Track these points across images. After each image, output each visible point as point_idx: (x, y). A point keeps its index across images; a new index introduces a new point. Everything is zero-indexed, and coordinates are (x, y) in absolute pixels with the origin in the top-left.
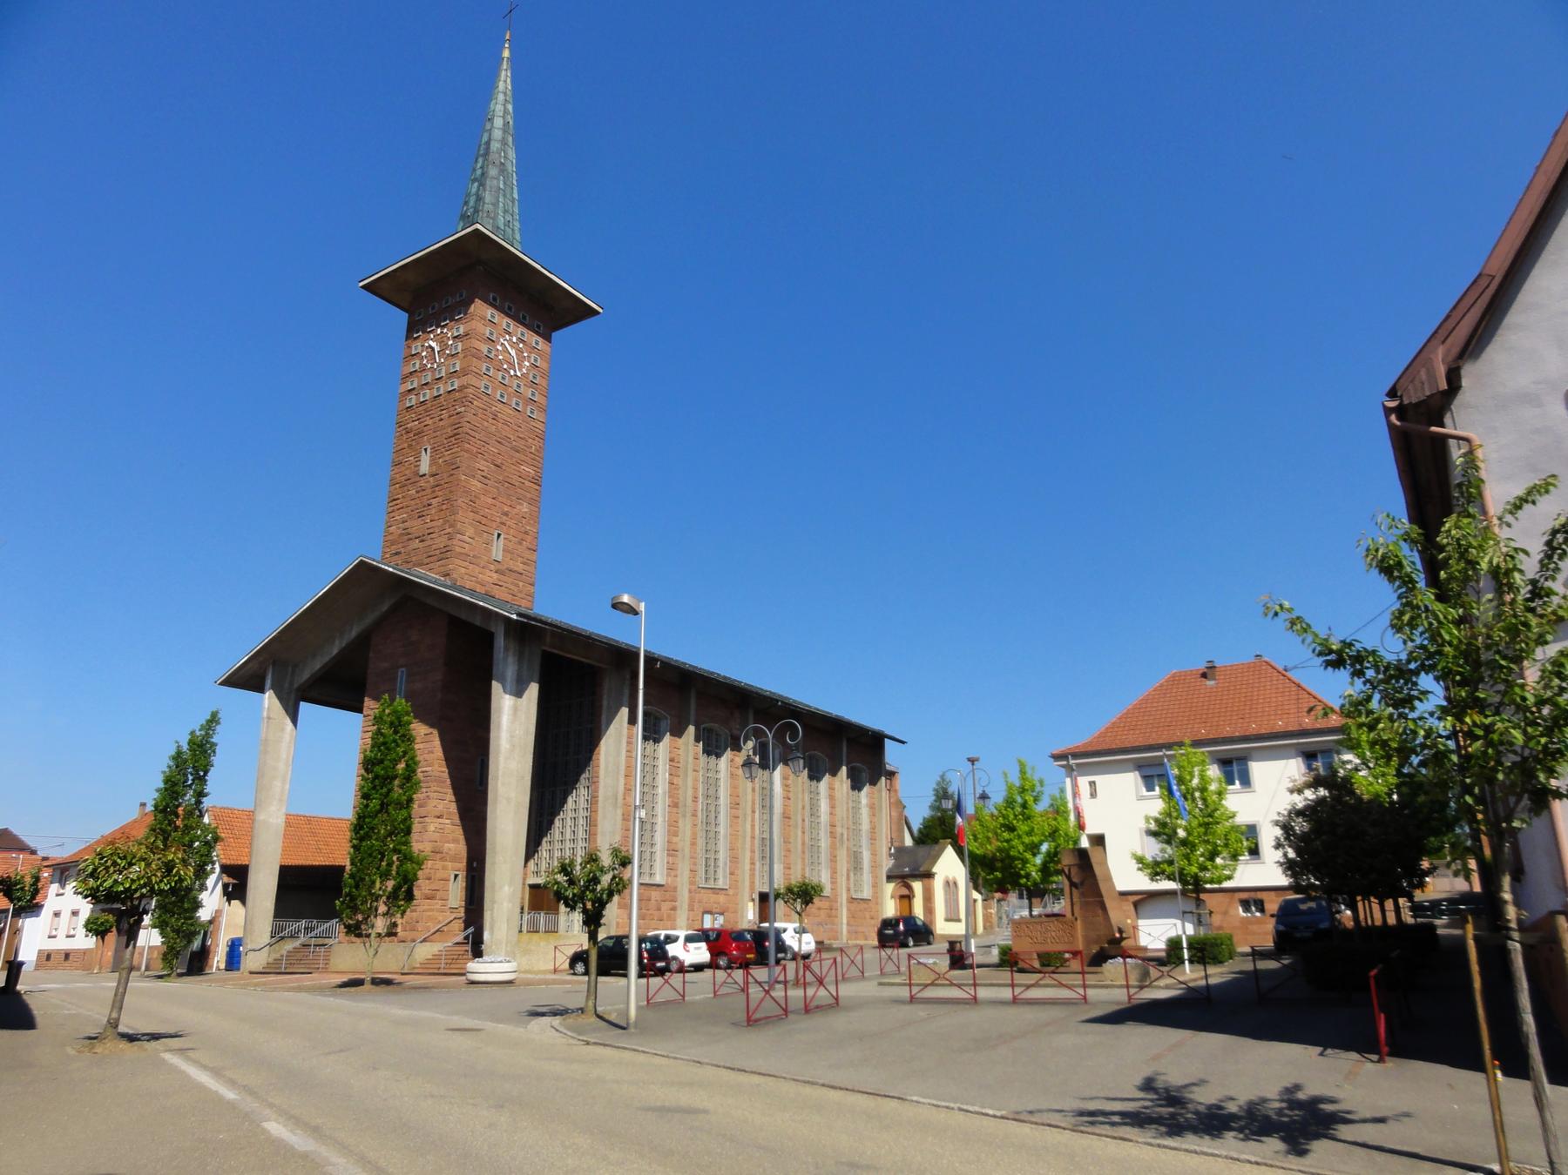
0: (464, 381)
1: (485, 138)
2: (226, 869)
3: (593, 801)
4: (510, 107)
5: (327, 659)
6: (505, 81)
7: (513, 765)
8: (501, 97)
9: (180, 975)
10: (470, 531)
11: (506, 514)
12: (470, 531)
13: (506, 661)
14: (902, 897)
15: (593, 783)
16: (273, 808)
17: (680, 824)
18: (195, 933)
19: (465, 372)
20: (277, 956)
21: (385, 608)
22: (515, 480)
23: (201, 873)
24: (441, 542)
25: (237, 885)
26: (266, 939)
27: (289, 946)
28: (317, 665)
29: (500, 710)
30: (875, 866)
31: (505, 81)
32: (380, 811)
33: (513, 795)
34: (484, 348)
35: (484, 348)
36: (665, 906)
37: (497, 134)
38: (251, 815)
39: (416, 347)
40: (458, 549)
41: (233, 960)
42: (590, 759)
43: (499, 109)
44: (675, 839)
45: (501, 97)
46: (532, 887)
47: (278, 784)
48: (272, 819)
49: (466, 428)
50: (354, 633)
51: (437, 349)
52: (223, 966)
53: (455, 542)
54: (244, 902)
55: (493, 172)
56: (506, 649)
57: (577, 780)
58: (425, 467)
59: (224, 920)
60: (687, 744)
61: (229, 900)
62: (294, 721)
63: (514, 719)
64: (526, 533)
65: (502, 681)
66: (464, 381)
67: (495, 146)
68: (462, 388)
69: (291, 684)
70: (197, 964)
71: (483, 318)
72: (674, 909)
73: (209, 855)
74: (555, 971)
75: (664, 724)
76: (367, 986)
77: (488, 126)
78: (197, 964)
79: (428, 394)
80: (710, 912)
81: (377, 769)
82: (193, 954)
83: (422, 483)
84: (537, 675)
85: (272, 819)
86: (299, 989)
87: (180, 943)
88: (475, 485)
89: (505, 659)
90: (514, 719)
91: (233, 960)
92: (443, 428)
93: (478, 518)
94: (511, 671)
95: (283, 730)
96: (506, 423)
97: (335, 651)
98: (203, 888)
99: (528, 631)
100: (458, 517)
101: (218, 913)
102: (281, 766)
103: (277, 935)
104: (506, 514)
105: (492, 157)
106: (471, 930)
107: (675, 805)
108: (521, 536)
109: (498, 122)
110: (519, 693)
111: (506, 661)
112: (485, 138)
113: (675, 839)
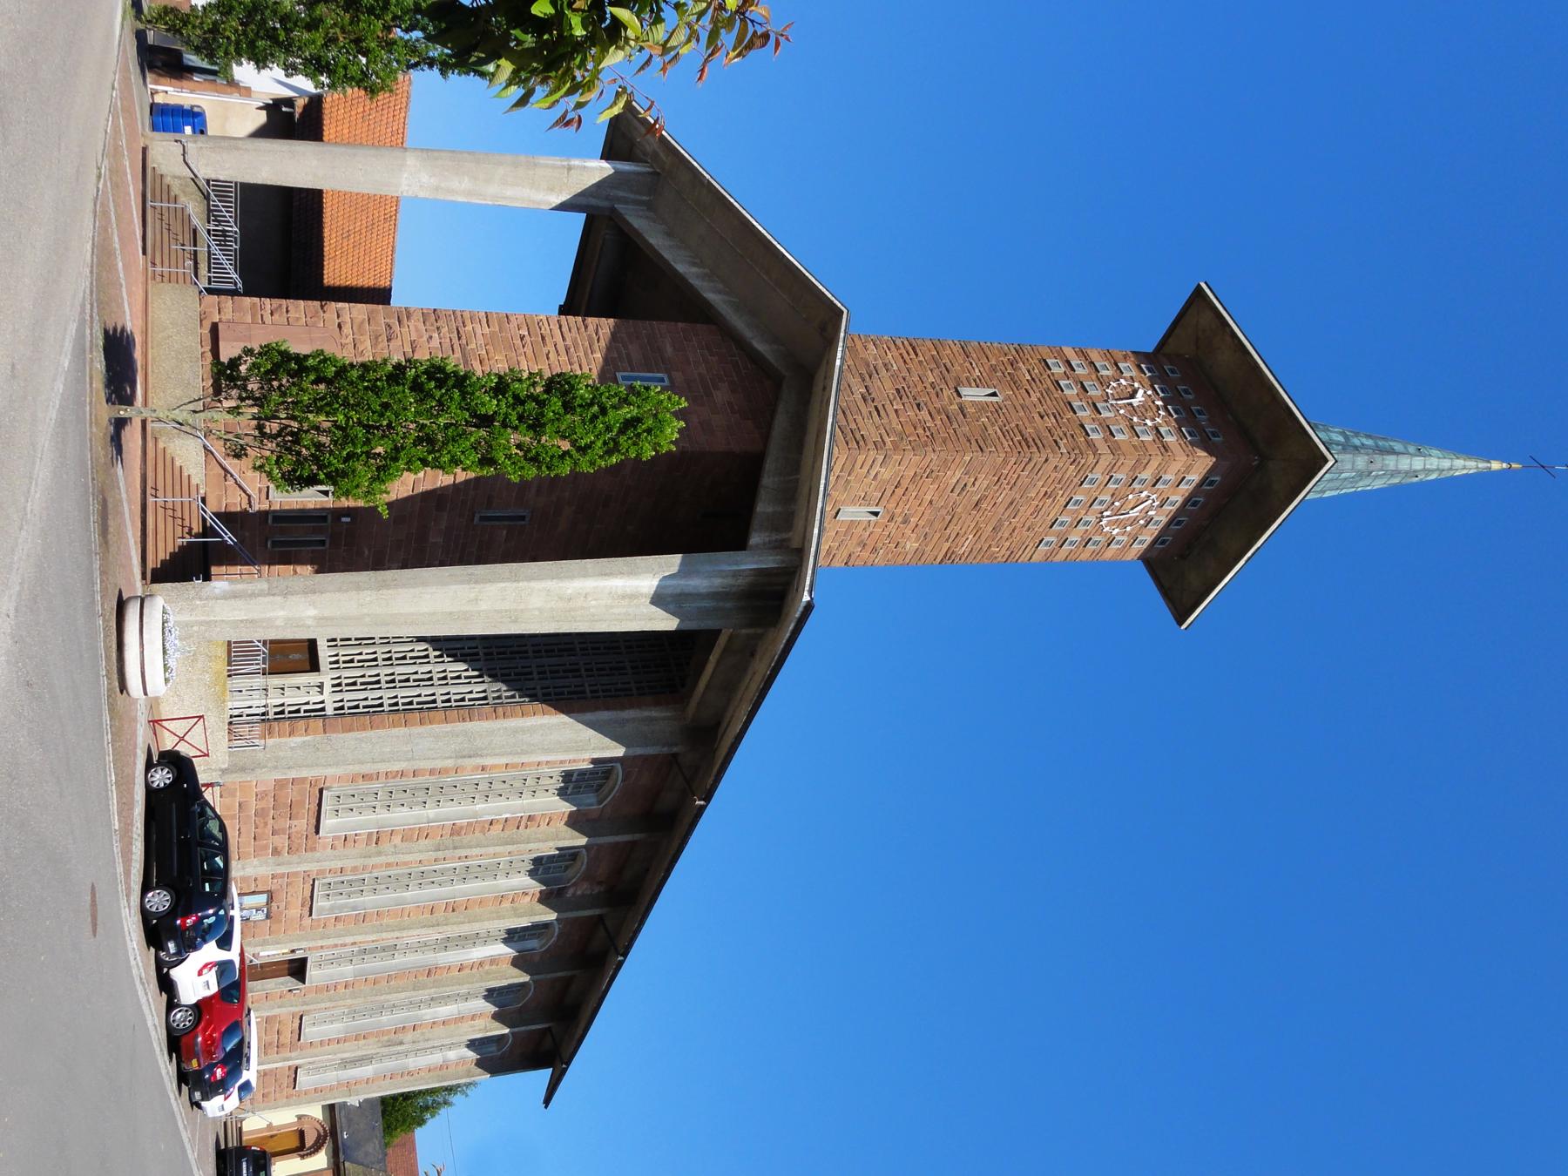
0: (1103, 449)
1: (1398, 447)
2: (315, 105)
3: (462, 708)
4: (1433, 476)
5: (666, 255)
6: (1465, 466)
7: (536, 601)
8: (1446, 464)
9: (140, 36)
10: (886, 473)
11: (906, 521)
12: (886, 473)
13: (720, 572)
14: (301, 1133)
15: (495, 707)
16: (424, 178)
17: (423, 843)
18: (211, 56)
19: (1115, 449)
20: (175, 190)
21: (760, 346)
22: (953, 529)
23: (316, 66)
24: (869, 429)
25: (291, 123)
26: (204, 172)
27: (194, 209)
28: (655, 238)
29: (632, 573)
30: (349, 1086)
31: (1465, 466)
32: (474, 415)
33: (484, 606)
34: (1146, 475)
35: (1146, 475)
36: (281, 841)
37: (1404, 463)
38: (397, 142)
39: (1128, 368)
40: (861, 458)
41: (168, 118)
42: (534, 697)
43: (1433, 463)
44: (397, 840)
45: (1446, 464)
46: (312, 644)
47: (466, 184)
48: (409, 178)
49: (1038, 458)
50: (711, 296)
51: (1135, 402)
52: (159, 99)
53: (873, 453)
54: (262, 133)
55: (1361, 461)
56: (736, 574)
57: (495, 677)
58: (972, 394)
59: (234, 100)
60: (557, 838)
61: (266, 107)
62: (563, 207)
63: (617, 595)
64: (874, 550)
65: (684, 572)
66: (1103, 449)
67: (1390, 461)
68: (1091, 445)
69: (625, 201)
70: (160, 60)
71: (1188, 469)
72: (276, 852)
73: (348, 79)
74: (155, 723)
75: (590, 799)
76: (106, 412)
77: (1412, 449)
78: (160, 60)
79: (1071, 392)
80: (271, 899)
81: (556, 404)
82: (178, 55)
83: (946, 392)
84: (692, 625)
85: (409, 178)
86: (103, 253)
87: (196, 35)
88: (954, 476)
89: (721, 574)
90: (617, 595)
91: (168, 118)
92: (1031, 420)
93: (905, 483)
94: (699, 584)
95: (551, 190)
96: (1037, 510)
97: (681, 268)
98: (290, 69)
99: (770, 605)
100: (909, 455)
101: (247, 92)
102: (493, 189)
103: (211, 191)
104: (906, 521)
105: (1378, 458)
106: (229, 538)
107: (456, 831)
108: (870, 543)
109: (1418, 463)
110: (658, 599)
111: (720, 572)
112: (1398, 447)
113: (397, 840)
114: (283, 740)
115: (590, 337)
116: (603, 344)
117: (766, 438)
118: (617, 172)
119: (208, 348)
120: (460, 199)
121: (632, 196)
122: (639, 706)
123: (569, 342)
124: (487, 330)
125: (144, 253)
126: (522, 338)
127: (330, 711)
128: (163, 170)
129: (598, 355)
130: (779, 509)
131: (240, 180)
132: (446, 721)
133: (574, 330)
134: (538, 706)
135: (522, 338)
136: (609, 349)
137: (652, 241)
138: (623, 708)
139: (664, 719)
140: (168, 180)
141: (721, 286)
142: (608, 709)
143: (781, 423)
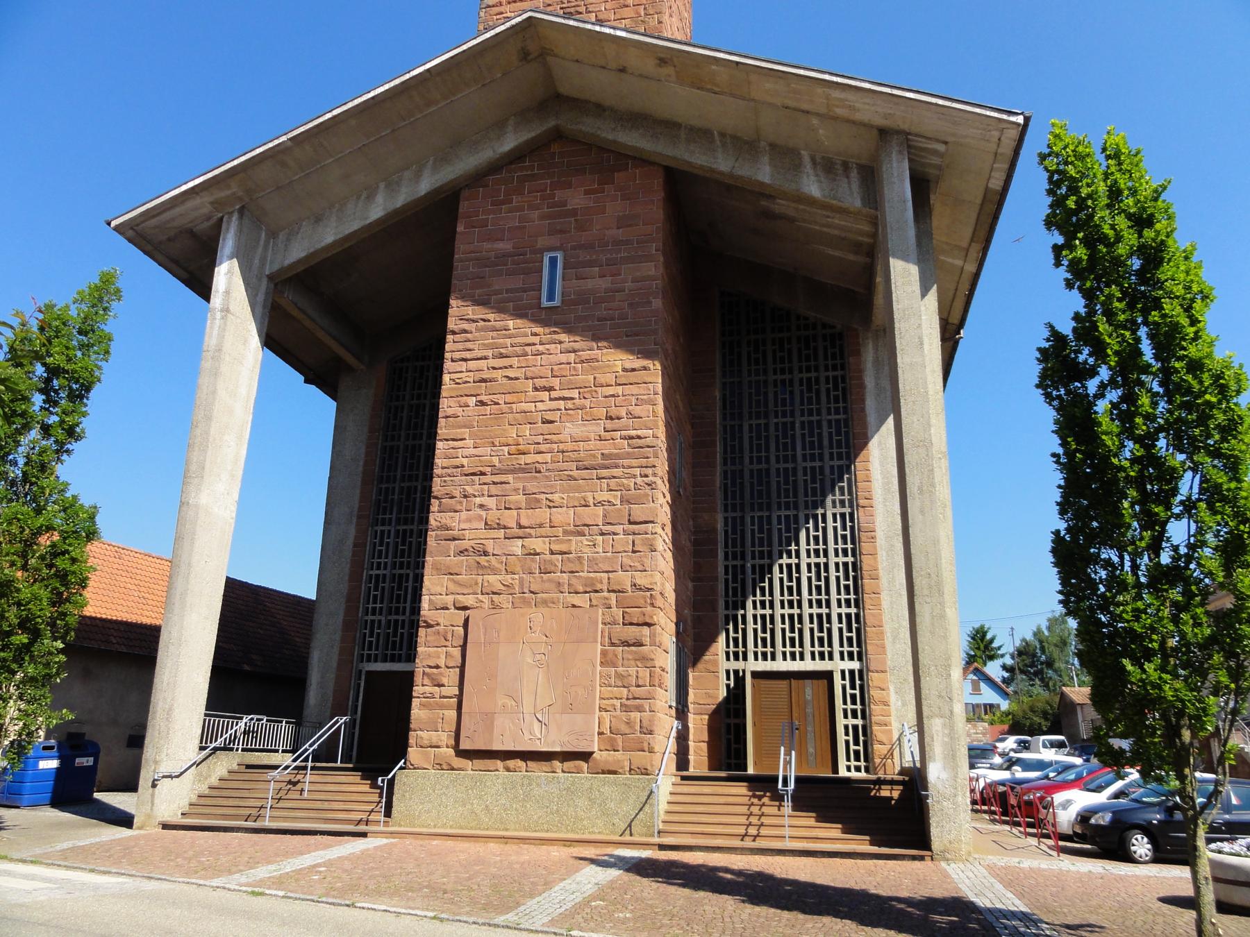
5: (355, 226)
21: (509, 143)
27: (223, 765)
114: (893, 712)
115: (478, 330)
116: (491, 316)
117: (642, 160)
118: (236, 254)
119: (499, 764)
120: (244, 452)
121: (260, 250)
122: (860, 371)
123: (490, 353)
124: (469, 442)
125: (364, 835)
126: (482, 403)
127: (855, 665)
128: (183, 804)
129: (511, 324)
130: (766, 159)
131: (202, 710)
132: (874, 554)
133: (469, 345)
134: (859, 464)
135: (482, 403)
136: (500, 310)
137: (329, 239)
138: (862, 386)
139: (876, 349)
140: (194, 799)
141: (407, 174)
142: (863, 401)
143: (632, 139)
